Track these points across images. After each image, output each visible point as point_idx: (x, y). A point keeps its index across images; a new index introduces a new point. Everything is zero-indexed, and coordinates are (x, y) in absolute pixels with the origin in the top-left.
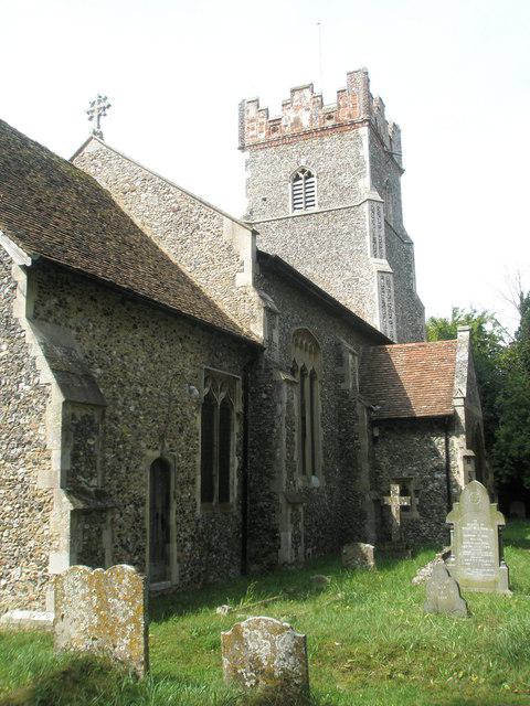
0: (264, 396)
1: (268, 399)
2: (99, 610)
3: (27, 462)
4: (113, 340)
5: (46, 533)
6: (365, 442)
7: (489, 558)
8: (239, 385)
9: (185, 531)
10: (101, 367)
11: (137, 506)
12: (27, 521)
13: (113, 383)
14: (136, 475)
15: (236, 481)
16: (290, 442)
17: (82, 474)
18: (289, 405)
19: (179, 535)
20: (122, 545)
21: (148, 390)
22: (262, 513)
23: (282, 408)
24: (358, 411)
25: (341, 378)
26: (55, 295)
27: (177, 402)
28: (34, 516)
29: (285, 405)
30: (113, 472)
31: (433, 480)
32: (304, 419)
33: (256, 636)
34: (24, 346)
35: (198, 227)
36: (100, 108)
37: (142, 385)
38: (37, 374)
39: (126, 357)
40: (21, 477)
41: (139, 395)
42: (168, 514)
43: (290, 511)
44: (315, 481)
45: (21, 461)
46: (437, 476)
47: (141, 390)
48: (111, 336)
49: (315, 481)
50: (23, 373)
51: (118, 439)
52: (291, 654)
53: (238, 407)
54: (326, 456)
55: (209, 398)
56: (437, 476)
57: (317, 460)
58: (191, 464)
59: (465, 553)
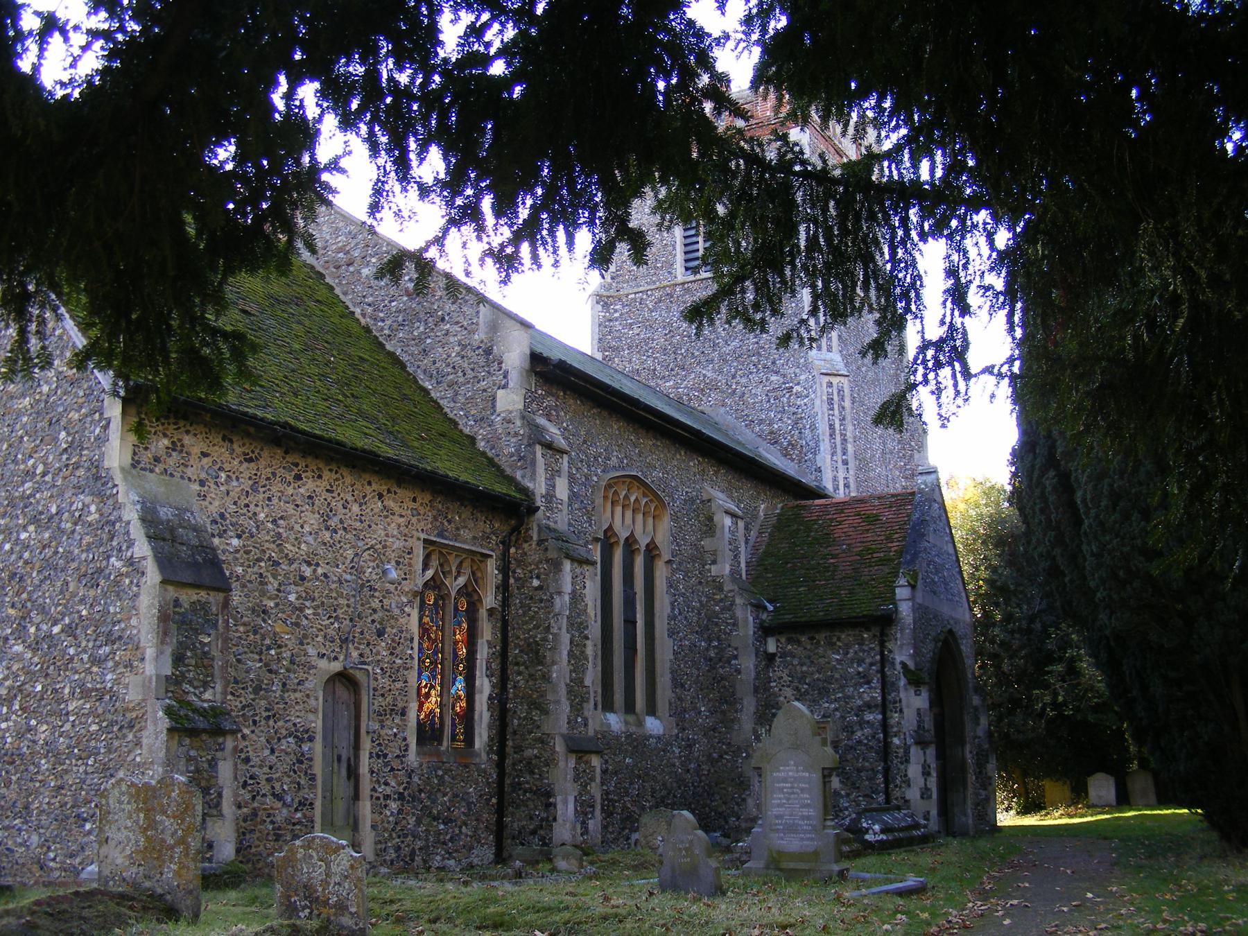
0: (536, 583)
1: (540, 588)
2: (146, 830)
3: (117, 664)
4: (261, 496)
5: (138, 759)
6: (748, 663)
7: (808, 818)
8: (491, 567)
9: (386, 784)
10: (239, 537)
11: (300, 741)
12: (116, 743)
13: (260, 560)
14: (298, 695)
15: (486, 716)
16: (577, 657)
17: (190, 683)
18: (576, 597)
19: (374, 790)
20: (273, 795)
21: (320, 571)
22: (530, 767)
23: (562, 602)
24: (739, 613)
25: (702, 558)
26: (165, 435)
27: (371, 589)
28: (125, 736)
29: (567, 598)
30: (257, 690)
31: (862, 724)
32: (630, 622)
33: (311, 857)
34: (117, 506)
35: (443, 319)
36: (723, 14)
37: (309, 564)
38: (131, 544)
39: (281, 522)
40: (109, 685)
41: (303, 578)
42: (357, 757)
43: (572, 764)
44: (653, 725)
45: (110, 664)
46: (869, 717)
47: (308, 572)
48: (256, 491)
49: (653, 725)
50: (114, 543)
51: (268, 642)
52: (346, 877)
53: (490, 599)
54: (677, 684)
55: (434, 584)
56: (869, 717)
57: (659, 692)
58: (399, 685)
59: (776, 811)
